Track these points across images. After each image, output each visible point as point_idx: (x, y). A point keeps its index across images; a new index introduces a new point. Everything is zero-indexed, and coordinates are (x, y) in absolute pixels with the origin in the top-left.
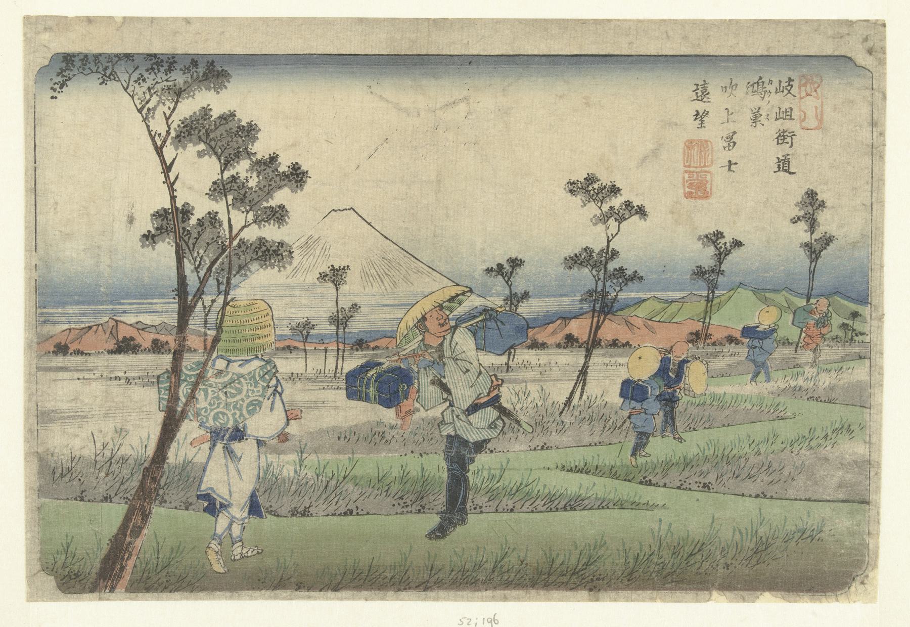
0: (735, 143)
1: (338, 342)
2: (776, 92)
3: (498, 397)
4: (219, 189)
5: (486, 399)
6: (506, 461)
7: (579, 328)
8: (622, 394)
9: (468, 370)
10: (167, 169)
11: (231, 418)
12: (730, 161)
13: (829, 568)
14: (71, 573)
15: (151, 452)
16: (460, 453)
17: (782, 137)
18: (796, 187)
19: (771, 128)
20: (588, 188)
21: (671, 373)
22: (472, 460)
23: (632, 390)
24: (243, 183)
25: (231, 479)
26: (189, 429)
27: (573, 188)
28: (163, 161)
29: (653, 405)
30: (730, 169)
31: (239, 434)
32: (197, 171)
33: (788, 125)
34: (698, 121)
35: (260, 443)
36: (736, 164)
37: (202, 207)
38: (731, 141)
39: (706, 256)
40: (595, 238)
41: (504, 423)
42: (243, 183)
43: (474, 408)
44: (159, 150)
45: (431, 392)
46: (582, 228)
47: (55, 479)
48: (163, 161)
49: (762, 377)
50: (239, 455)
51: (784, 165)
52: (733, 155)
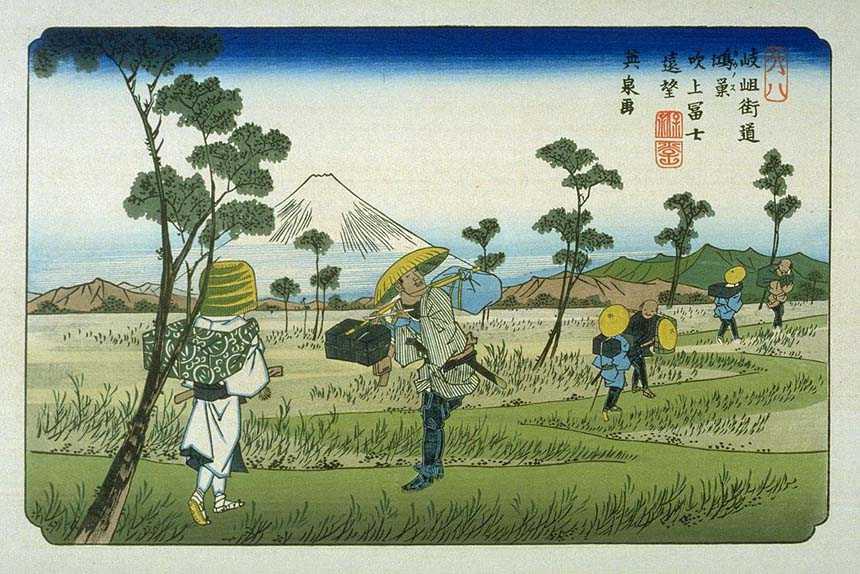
0: (701, 112)
1: (317, 301)
2: (742, 65)
3: (474, 353)
4: (199, 156)
5: (462, 356)
6: (478, 404)
7: (555, 290)
8: (596, 351)
9: (443, 329)
10: (151, 135)
11: (213, 373)
12: (696, 130)
13: (786, 510)
14: (61, 519)
15: (90, 499)
16: (436, 409)
17: (747, 106)
18: (755, 156)
19: (737, 96)
20: (561, 153)
21: (642, 328)
22: (447, 415)
23: (604, 346)
24: (569, 225)
25: (213, 432)
26: (171, 386)
27: (546, 153)
28: (148, 127)
29: (621, 360)
30: (696, 138)
31: (221, 392)
32: (180, 142)
33: (752, 96)
34: (665, 91)
35: (242, 399)
36: (703, 132)
37: (186, 171)
38: (696, 113)
39: (673, 219)
40: (568, 201)
41: (479, 381)
42: (569, 225)
43: (450, 365)
44: (144, 115)
45: (406, 352)
46: (553, 191)
47: (48, 426)
48: (148, 127)
49: (729, 333)
50: (209, 455)
51: (748, 133)
52: (699, 124)
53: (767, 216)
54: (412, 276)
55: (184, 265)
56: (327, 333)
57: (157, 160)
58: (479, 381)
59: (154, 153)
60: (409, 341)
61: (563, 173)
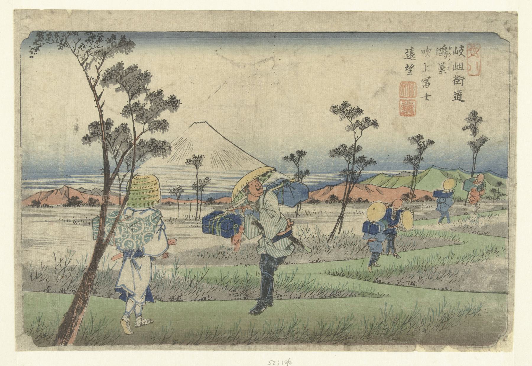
0: (429, 84)
1: (197, 199)
3: (291, 232)
4: (128, 111)
5: (284, 233)
7: (338, 191)
8: (364, 230)
10: (98, 98)
11: (135, 244)
12: (427, 94)
13: (484, 332)
14: (42, 334)
15: (88, 263)
16: (269, 264)
17: (457, 80)
18: (463, 110)
19: (450, 75)
20: (344, 110)
21: (392, 218)
23: (369, 228)
25: (135, 279)
26: (110, 251)
27: (335, 110)
28: (95, 94)
29: (382, 237)
30: (426, 99)
31: (140, 253)
32: (115, 100)
33: (460, 73)
34: (408, 71)
35: (152, 258)
36: (430, 95)
37: (118, 121)
38: (427, 82)
39: (413, 149)
40: (348, 139)
41: (295, 247)
43: (277, 238)
44: (93, 88)
45: (252, 229)
46: (340, 133)
47: (32, 280)
48: (95, 94)
49: (445, 220)
51: (458, 96)
52: (428, 90)
53: (74, 208)
54: (254, 184)
55: (117, 177)
56: (203, 218)
57: (101, 116)
58: (295, 247)
59: (100, 109)
60: (253, 223)
61: (346, 122)
